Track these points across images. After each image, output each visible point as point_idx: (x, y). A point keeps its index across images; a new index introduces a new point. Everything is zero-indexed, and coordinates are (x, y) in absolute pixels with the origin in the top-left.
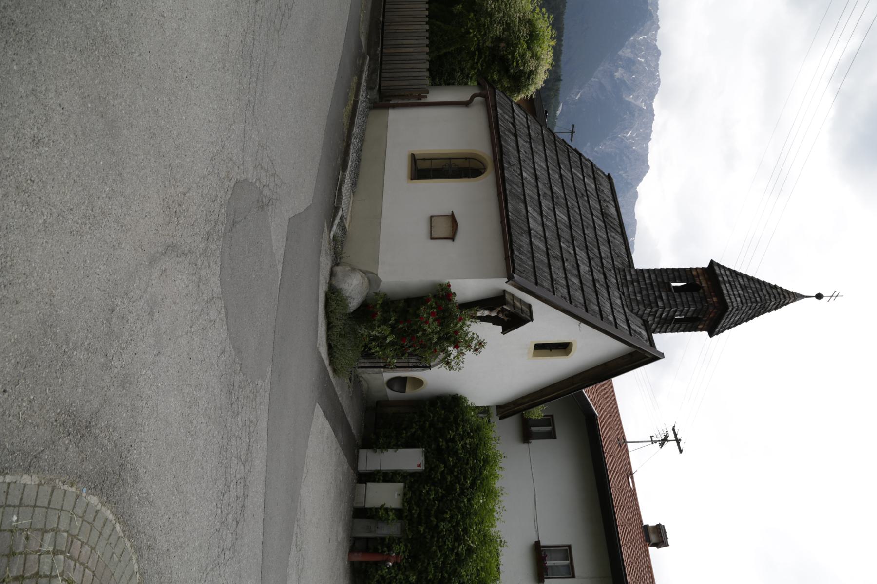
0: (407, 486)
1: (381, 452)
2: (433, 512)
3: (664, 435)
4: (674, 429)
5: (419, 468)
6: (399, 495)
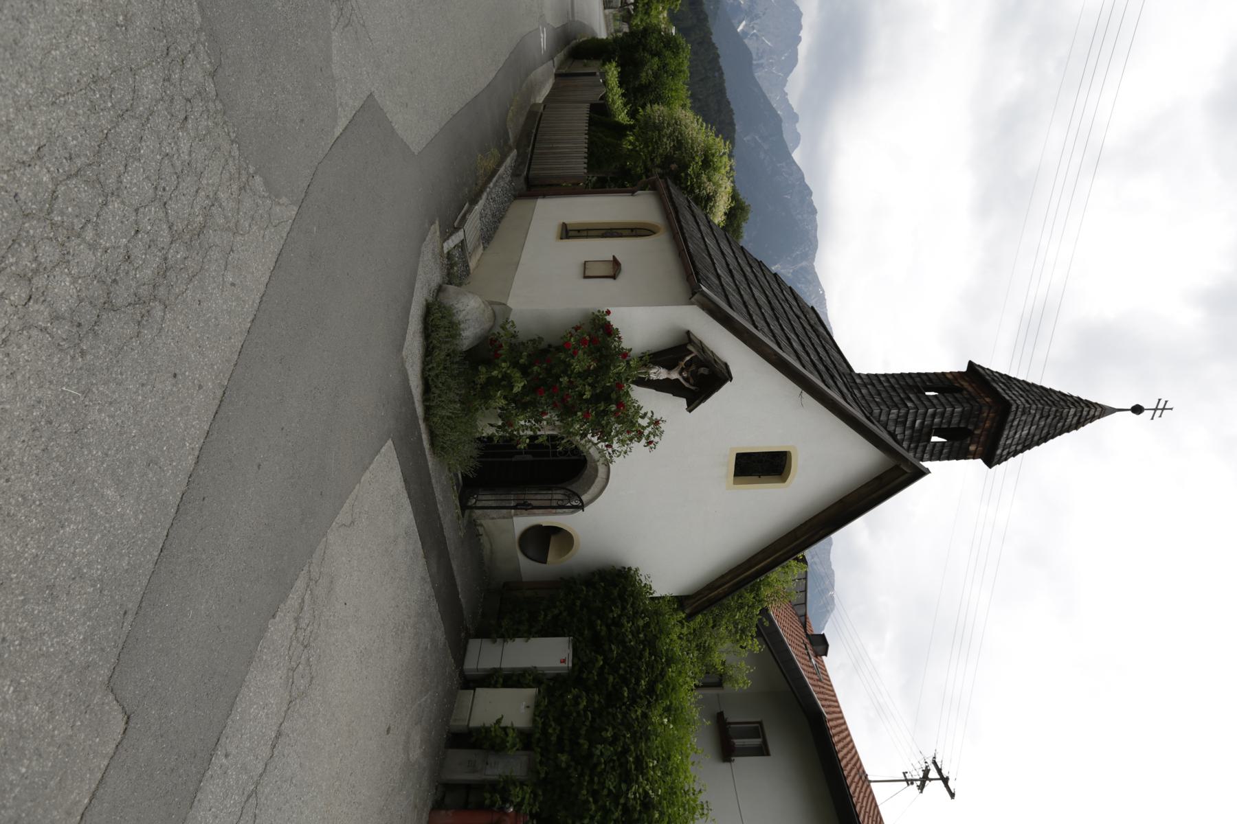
0: (542, 691)
1: (504, 641)
2: (583, 732)
3: (923, 770)
4: (935, 763)
5: (563, 665)
6: (528, 707)
